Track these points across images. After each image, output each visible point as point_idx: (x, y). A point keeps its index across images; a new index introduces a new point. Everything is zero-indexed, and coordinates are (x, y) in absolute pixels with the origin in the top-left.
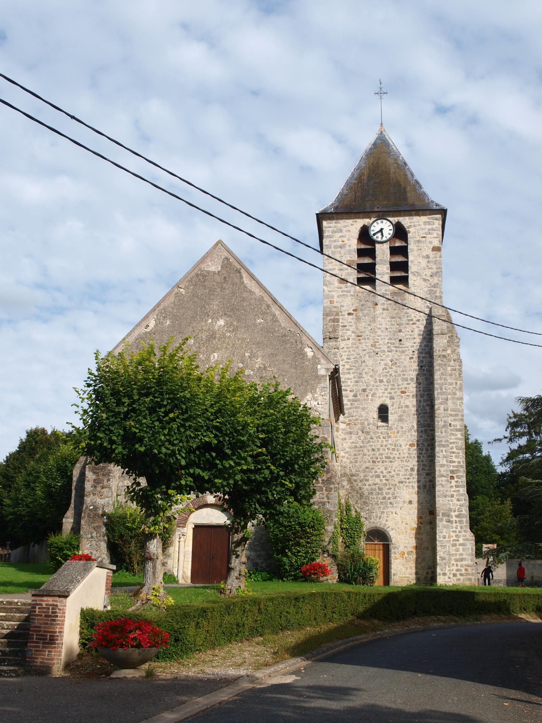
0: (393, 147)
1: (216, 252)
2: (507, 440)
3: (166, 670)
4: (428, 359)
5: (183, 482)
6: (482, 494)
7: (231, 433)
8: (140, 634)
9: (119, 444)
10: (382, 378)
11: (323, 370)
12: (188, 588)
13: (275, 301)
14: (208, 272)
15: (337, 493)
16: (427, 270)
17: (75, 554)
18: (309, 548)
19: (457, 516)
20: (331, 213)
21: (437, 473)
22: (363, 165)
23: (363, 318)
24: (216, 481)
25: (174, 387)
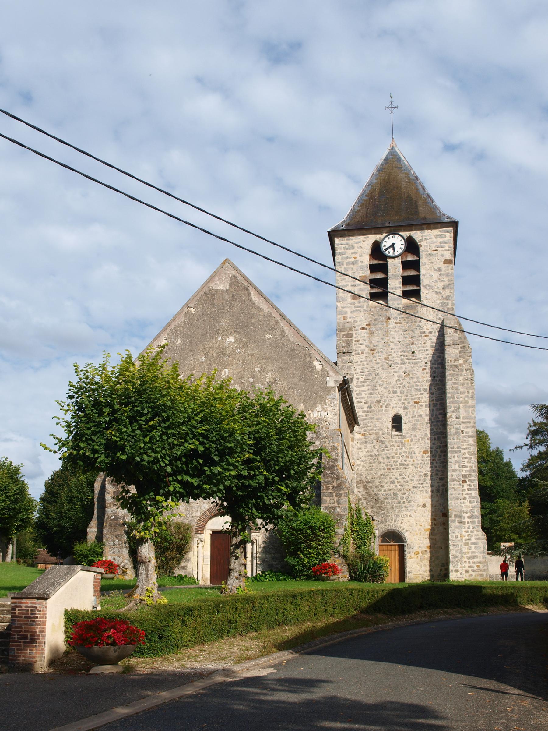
0: (405, 161)
1: (224, 270)
2: (528, 447)
3: (143, 665)
4: (441, 370)
5: (171, 489)
6: (502, 497)
7: (217, 440)
8: (115, 633)
9: (102, 453)
10: (395, 389)
11: (333, 381)
12: (206, 588)
13: (283, 317)
14: (217, 291)
15: (347, 499)
16: (439, 283)
17: (99, 560)
18: (320, 549)
19: (468, 517)
20: (343, 230)
21: (449, 477)
22: (375, 181)
23: (377, 332)
24: (205, 486)
25: (154, 395)
